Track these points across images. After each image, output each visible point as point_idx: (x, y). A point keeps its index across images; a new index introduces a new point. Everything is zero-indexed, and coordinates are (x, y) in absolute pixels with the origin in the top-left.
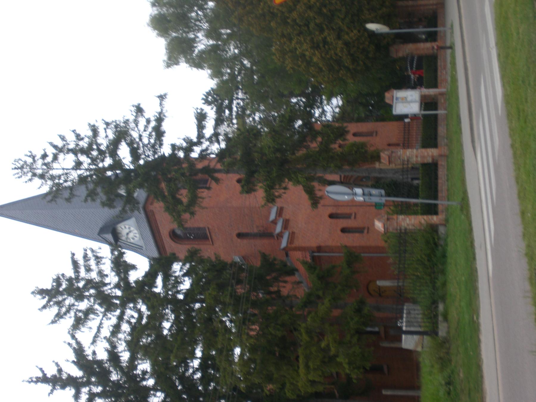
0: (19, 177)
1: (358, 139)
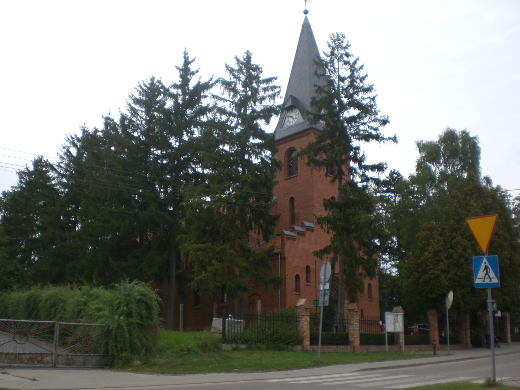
0: (331, 38)
1: (366, 286)
